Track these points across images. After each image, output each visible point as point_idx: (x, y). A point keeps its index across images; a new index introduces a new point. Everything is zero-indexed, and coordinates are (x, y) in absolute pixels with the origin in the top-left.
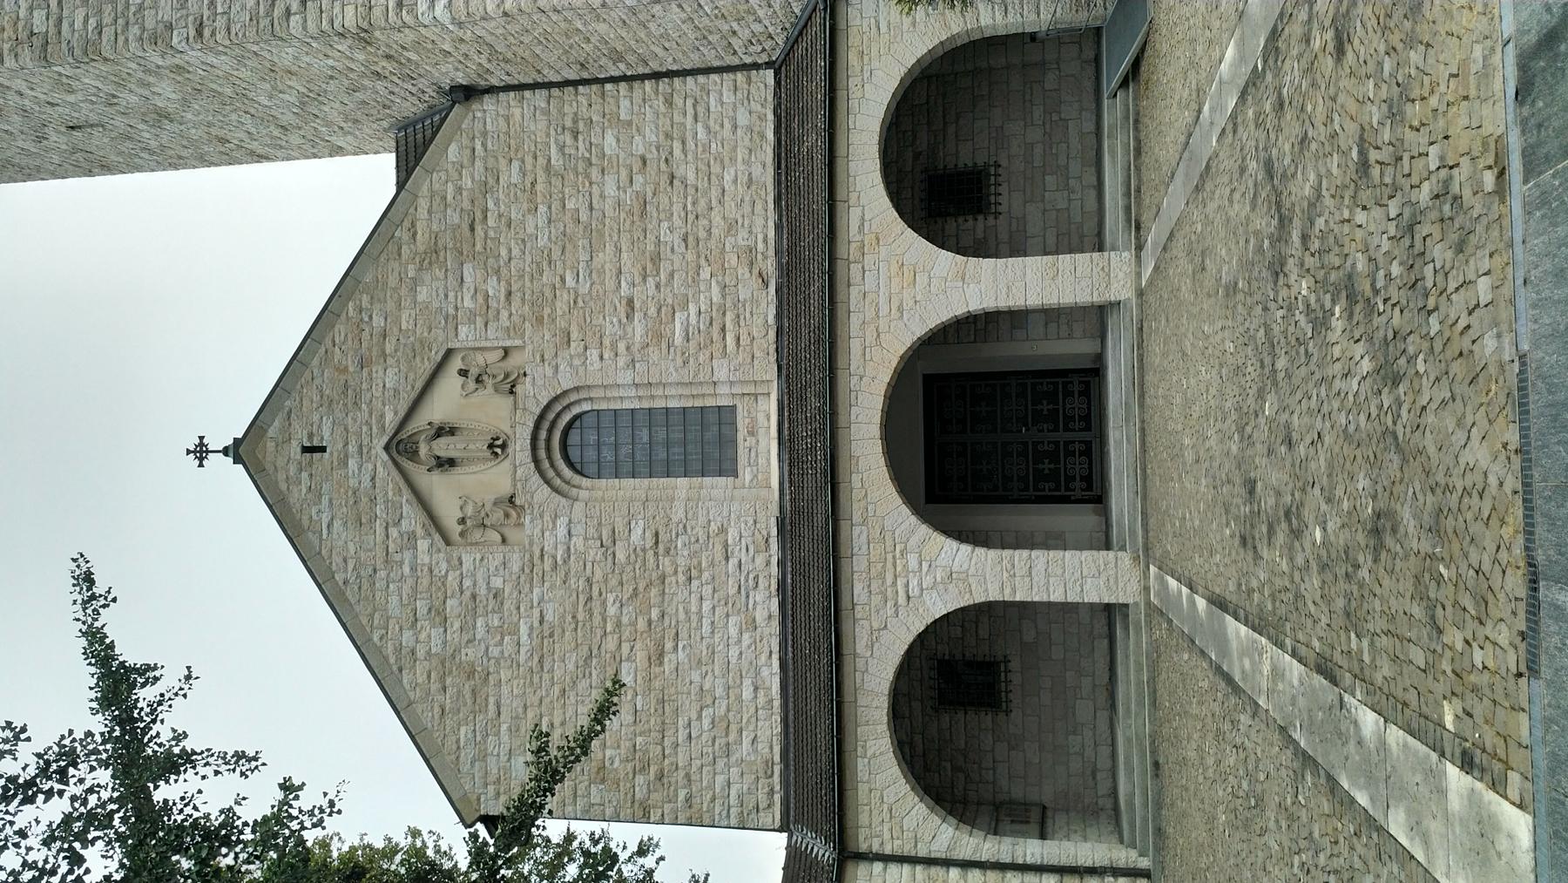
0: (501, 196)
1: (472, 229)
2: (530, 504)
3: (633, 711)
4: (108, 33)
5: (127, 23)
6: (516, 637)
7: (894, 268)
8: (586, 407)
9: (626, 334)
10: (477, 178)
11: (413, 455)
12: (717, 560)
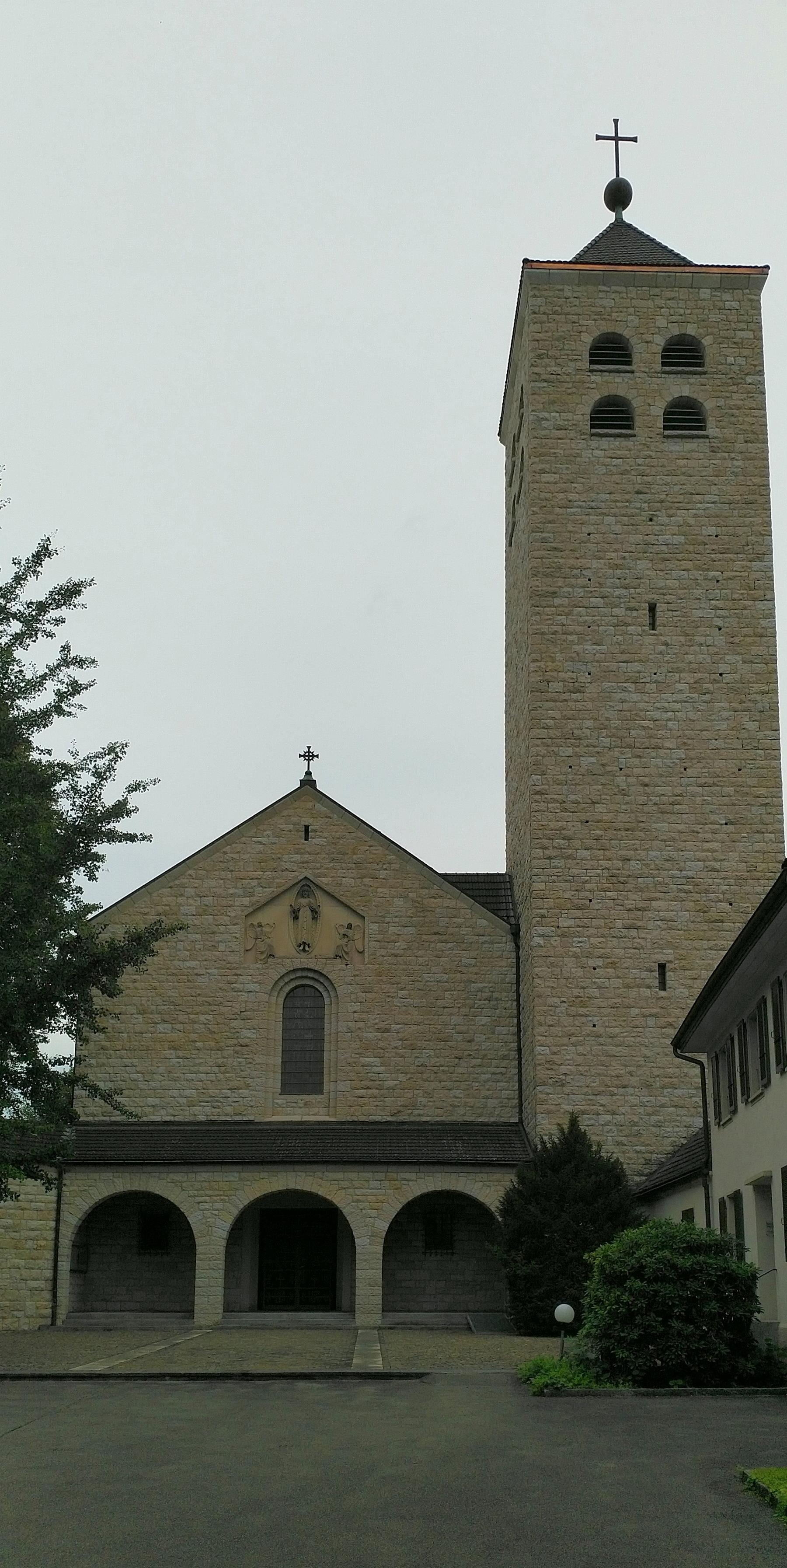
0: (455, 952)
1: (436, 934)
2: (268, 967)
3: (143, 1031)
4: (543, 733)
5: (548, 746)
6: (188, 959)
7: (381, 1198)
8: (327, 1001)
9: (368, 1027)
10: (466, 937)
11: (302, 894)
12: (229, 1083)
